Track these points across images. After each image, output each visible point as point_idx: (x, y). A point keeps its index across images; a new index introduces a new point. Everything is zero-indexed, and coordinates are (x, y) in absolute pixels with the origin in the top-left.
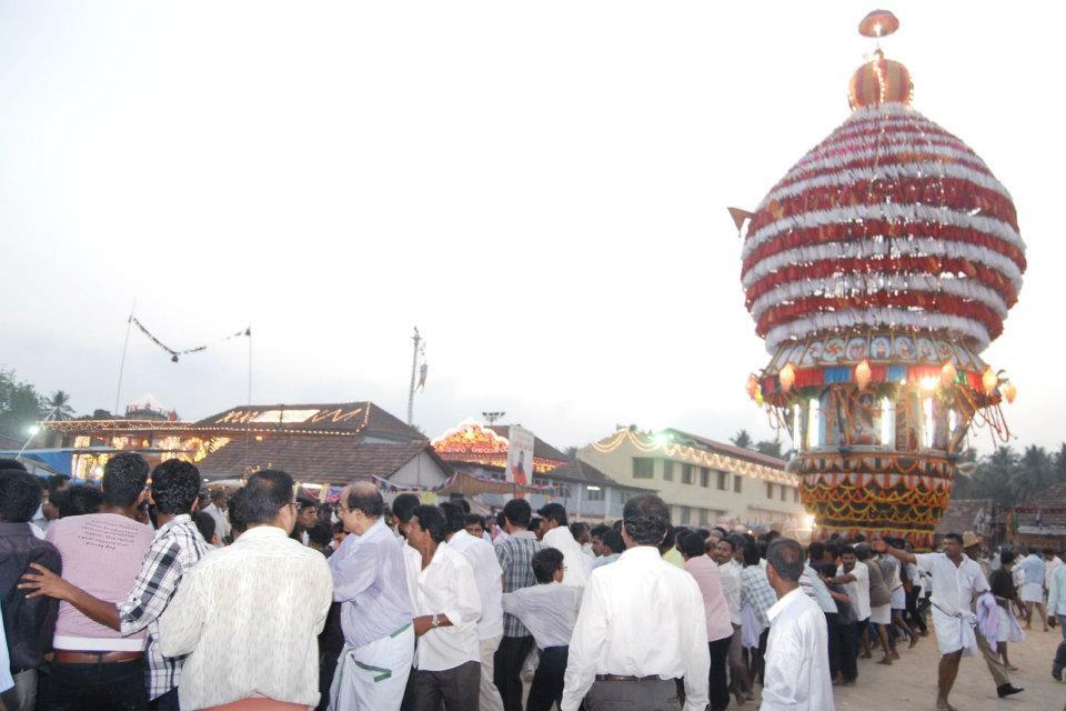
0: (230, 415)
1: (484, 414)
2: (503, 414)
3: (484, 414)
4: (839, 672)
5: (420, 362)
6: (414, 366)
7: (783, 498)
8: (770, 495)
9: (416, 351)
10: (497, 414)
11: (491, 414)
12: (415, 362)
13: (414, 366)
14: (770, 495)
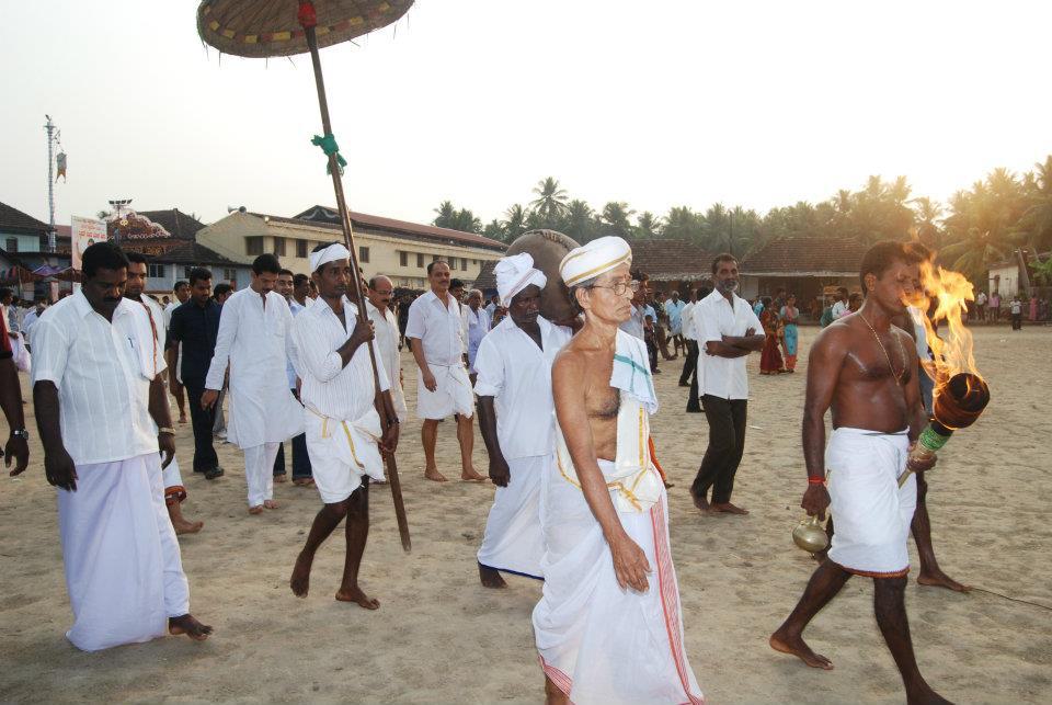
0: (138, 700)
1: (111, 202)
2: (129, 202)
3: (111, 202)
4: (541, 321)
5: (57, 151)
6: (51, 156)
7: (464, 268)
8: (404, 262)
9: (50, 139)
10: (123, 202)
11: (118, 202)
12: (50, 152)
13: (51, 156)
14: (404, 262)
